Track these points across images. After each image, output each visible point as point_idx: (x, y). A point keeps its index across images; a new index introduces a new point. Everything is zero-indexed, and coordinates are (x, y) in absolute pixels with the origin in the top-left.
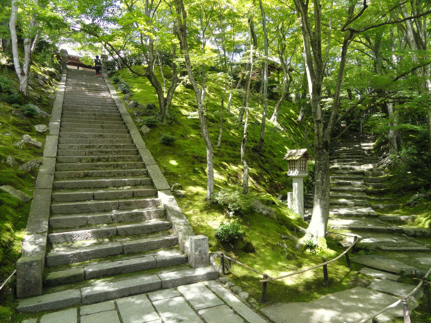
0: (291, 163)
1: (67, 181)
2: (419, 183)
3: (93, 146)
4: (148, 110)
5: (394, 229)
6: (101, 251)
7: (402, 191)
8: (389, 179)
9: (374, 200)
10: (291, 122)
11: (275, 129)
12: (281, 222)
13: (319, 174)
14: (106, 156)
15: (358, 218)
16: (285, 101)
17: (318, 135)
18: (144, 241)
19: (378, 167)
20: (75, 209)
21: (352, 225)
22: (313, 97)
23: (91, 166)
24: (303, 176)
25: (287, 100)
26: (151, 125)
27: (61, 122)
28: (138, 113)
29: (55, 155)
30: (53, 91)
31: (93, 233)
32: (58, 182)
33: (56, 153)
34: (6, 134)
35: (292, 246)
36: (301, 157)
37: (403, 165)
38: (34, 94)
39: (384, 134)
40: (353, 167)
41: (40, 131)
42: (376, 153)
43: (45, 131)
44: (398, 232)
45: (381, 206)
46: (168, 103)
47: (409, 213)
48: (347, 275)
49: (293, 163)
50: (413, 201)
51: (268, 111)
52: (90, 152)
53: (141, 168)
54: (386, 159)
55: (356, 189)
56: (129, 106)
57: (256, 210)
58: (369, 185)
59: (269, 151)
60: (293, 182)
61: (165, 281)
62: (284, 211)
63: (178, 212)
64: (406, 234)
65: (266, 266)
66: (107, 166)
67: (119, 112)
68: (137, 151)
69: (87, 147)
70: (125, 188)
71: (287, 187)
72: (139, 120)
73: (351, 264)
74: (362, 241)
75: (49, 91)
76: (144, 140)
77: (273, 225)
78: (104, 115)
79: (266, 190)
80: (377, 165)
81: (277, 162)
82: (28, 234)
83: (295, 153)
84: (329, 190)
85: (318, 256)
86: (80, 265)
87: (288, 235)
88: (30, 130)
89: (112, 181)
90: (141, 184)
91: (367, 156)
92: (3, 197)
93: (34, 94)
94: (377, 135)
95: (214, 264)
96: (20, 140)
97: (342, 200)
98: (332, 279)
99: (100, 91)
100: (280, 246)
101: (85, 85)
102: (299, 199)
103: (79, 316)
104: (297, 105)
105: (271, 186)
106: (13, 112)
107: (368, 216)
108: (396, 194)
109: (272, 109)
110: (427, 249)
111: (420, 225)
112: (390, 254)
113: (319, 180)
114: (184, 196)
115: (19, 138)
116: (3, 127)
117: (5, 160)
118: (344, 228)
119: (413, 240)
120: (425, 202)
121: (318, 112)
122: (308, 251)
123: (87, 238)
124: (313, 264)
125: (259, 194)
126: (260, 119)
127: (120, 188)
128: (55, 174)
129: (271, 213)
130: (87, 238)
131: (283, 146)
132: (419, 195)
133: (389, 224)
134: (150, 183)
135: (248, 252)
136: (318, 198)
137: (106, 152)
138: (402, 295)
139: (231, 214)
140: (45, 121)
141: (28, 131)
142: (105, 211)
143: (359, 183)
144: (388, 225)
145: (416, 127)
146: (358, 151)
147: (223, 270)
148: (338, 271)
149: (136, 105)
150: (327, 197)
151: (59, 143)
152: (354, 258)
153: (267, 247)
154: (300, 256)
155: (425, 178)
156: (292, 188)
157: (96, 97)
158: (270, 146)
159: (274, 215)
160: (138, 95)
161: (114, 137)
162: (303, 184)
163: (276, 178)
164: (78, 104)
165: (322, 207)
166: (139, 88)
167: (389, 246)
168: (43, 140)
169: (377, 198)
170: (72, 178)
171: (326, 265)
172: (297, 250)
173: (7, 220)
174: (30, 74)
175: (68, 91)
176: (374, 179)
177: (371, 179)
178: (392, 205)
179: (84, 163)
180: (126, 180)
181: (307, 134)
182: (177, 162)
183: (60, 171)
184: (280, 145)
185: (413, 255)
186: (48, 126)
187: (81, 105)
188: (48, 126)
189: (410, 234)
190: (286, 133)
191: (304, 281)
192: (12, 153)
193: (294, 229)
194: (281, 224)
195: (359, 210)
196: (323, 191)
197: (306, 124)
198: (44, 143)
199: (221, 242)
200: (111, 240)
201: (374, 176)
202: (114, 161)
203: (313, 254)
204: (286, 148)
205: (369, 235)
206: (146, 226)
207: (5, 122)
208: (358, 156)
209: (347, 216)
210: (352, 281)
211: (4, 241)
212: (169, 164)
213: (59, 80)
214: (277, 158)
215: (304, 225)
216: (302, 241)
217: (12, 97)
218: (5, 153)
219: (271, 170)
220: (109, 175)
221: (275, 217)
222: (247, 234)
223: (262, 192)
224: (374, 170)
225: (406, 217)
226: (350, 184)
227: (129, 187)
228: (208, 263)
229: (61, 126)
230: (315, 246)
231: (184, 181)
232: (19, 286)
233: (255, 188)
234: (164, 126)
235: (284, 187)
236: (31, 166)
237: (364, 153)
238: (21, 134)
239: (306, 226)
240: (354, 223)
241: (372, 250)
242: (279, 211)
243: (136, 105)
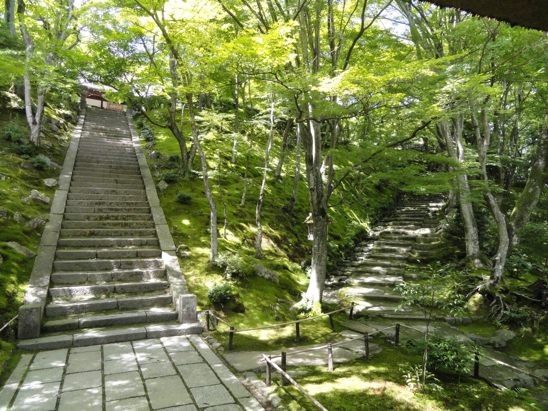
1: (72, 239)
3: (103, 203)
4: (169, 163)
6: (96, 305)
12: (284, 286)
14: (116, 214)
18: (137, 298)
20: (77, 267)
23: (98, 224)
26: (170, 181)
27: (73, 175)
28: (159, 166)
29: (62, 212)
30: (67, 138)
31: (92, 289)
32: (62, 240)
33: (63, 210)
34: (14, 189)
38: (46, 142)
41: (49, 185)
43: (54, 185)
46: (191, 156)
52: (99, 209)
53: (150, 228)
56: (151, 156)
57: (259, 274)
61: (150, 332)
63: (176, 272)
66: (115, 225)
67: (138, 164)
68: (150, 209)
69: (96, 204)
70: (130, 247)
72: (158, 174)
75: (63, 138)
76: (159, 197)
78: (121, 168)
79: (288, 255)
80: (435, 229)
82: (31, 287)
86: (76, 316)
88: (39, 185)
89: (117, 240)
90: (147, 244)
92: (9, 252)
93: (46, 142)
95: (201, 321)
96: (27, 196)
99: (120, 137)
101: (105, 130)
103: (69, 353)
105: (296, 250)
106: (22, 164)
114: (189, 258)
115: (27, 193)
116: (12, 182)
117: (12, 217)
118: (358, 296)
123: (85, 294)
127: (125, 248)
128: (60, 232)
130: (85, 294)
134: (156, 243)
135: (238, 312)
137: (117, 210)
139: (229, 276)
140: (55, 174)
141: (37, 185)
142: (106, 269)
143: (404, 250)
147: (208, 325)
149: (158, 156)
151: (68, 198)
157: (115, 145)
160: (162, 143)
161: (128, 193)
164: (94, 154)
165: (317, 273)
166: (164, 135)
168: (52, 195)
170: (78, 236)
173: (12, 273)
174: (43, 119)
175: (85, 138)
177: (423, 246)
179: (92, 221)
180: (132, 239)
182: (190, 222)
183: (67, 228)
186: (58, 180)
187: (96, 154)
188: (58, 180)
192: (19, 209)
194: (283, 289)
195: (386, 279)
198: (52, 199)
199: (213, 302)
200: (108, 296)
202: (124, 219)
206: (143, 285)
207: (14, 175)
208: (418, 218)
211: (8, 292)
212: (182, 224)
213: (75, 124)
216: (298, 305)
217: (22, 148)
218: (13, 209)
220: (116, 234)
222: (241, 295)
226: (395, 251)
227: (134, 246)
228: (196, 320)
229: (72, 180)
231: (193, 242)
232: (20, 329)
234: (185, 181)
236: (37, 222)
237: (428, 216)
238: (29, 189)
243: (158, 156)
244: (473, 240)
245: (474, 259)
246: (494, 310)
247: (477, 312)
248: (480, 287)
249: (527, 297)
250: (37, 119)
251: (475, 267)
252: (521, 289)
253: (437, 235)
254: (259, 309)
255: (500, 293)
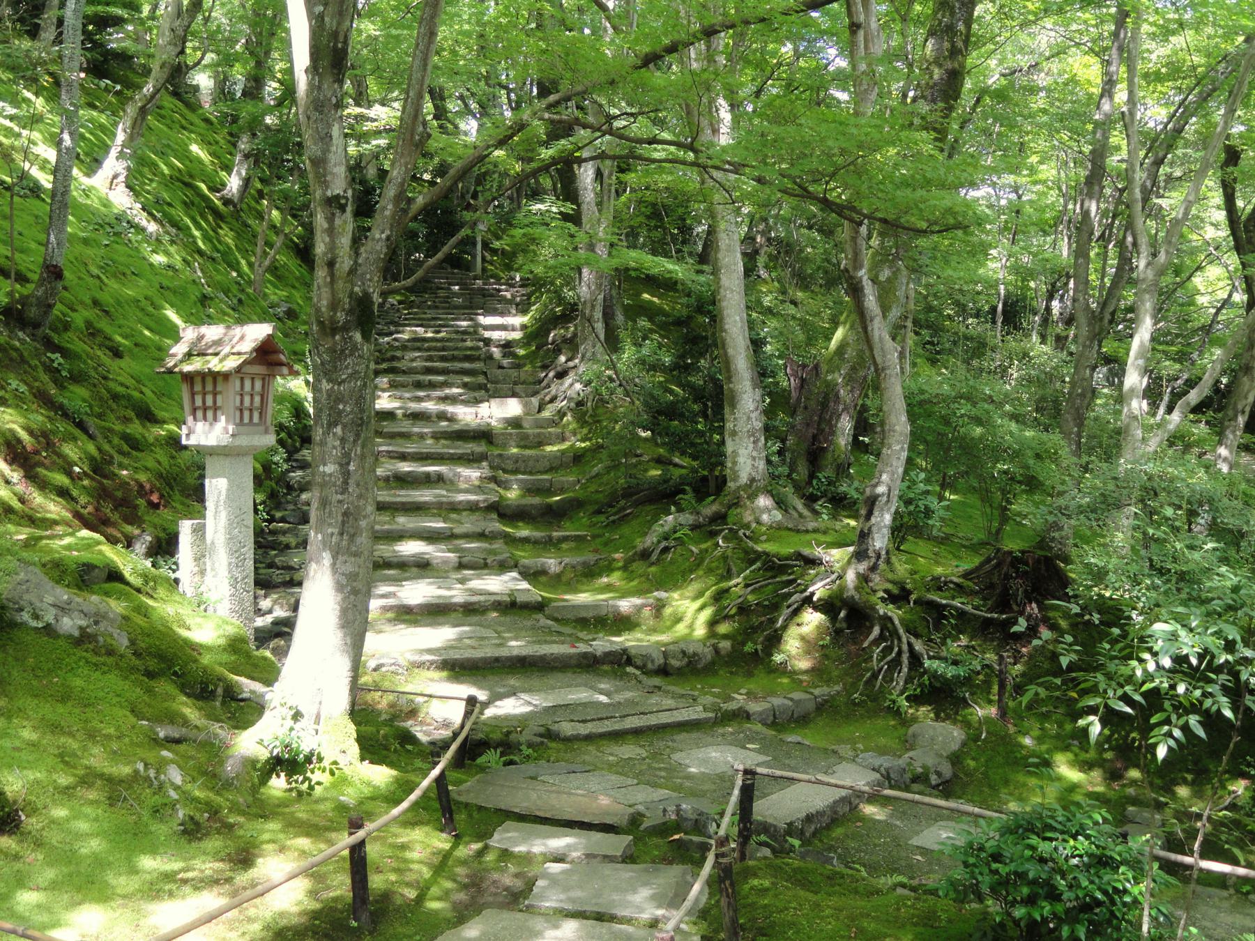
0: (198, 388)
2: (676, 473)
5: (598, 654)
7: (622, 503)
8: (578, 458)
9: (525, 540)
10: (197, 200)
11: (116, 226)
12: (153, 664)
13: (330, 439)
15: (475, 619)
16: (168, 102)
17: (331, 264)
19: (539, 411)
21: (452, 647)
22: (311, 86)
24: (255, 448)
25: (176, 94)
35: (205, 773)
36: (245, 363)
37: (622, 404)
39: (562, 285)
40: (450, 409)
42: (531, 357)
44: (612, 663)
45: (552, 563)
47: (646, 586)
48: (442, 864)
49: (209, 387)
50: (659, 542)
51: (82, 137)
54: (568, 381)
55: (461, 497)
57: (25, 617)
58: (507, 481)
59: (89, 324)
60: (208, 472)
62: (165, 608)
64: (637, 667)
65: (79, 890)
71: (177, 496)
73: (456, 817)
74: (489, 712)
77: (113, 680)
79: (77, 515)
80: (535, 401)
81: (131, 382)
83: (218, 342)
84: (370, 509)
85: (319, 801)
87: (186, 722)
91: (501, 367)
94: (534, 284)
97: (410, 548)
98: (386, 896)
100: (147, 779)
102: (234, 551)
104: (222, 123)
105: (102, 494)
107: (511, 607)
108: (602, 518)
109: (102, 127)
110: (704, 715)
111: (681, 629)
112: (590, 753)
113: (330, 468)
118: (420, 665)
119: (659, 688)
120: (697, 543)
121: (332, 158)
122: (278, 784)
124: (303, 842)
125: (39, 533)
126: (42, 168)
129: (102, 626)
131: (157, 307)
132: (675, 519)
133: (582, 635)
136: (325, 544)
138: (642, 910)
143: (472, 474)
144: (579, 640)
145: (670, 266)
146: (469, 344)
148: (409, 855)
150: (363, 540)
152: (466, 789)
153: (80, 791)
154: (242, 813)
155: (695, 458)
156: (201, 499)
158: (96, 303)
159: (116, 632)
162: (250, 483)
163: (121, 452)
165: (340, 587)
167: (584, 721)
169: (537, 534)
171: (362, 844)
172: (228, 785)
176: (525, 460)
177: (516, 459)
178: (591, 557)
181: (267, 263)
184: (144, 303)
185: (662, 744)
189: (650, 666)
190: (172, 249)
191: (267, 928)
193: (213, 692)
194: (150, 675)
195: (476, 584)
196: (346, 514)
197: (260, 216)
201: (525, 447)
203: (300, 794)
204: (171, 315)
205: (513, 681)
208: (467, 365)
209: (435, 612)
210: (465, 887)
214: (123, 363)
215: (255, 666)
219: (100, 416)
221: (123, 642)
223: (56, 522)
224: (525, 425)
225: (637, 601)
226: (439, 479)
230: (308, 760)
233: (16, 504)
235: (162, 496)
237: (490, 357)
239: (269, 675)
240: (460, 639)
241: (530, 745)
242: (143, 611)
244: (751, 433)
245: (753, 497)
246: (879, 661)
247: (817, 672)
248: (819, 590)
249: (969, 608)
251: (758, 522)
252: (946, 583)
253: (553, 423)
254: (92, 795)
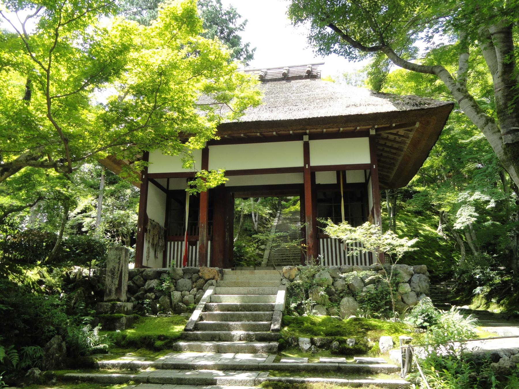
213: (274, 217)
250: (257, 219)
255: (471, 195)
